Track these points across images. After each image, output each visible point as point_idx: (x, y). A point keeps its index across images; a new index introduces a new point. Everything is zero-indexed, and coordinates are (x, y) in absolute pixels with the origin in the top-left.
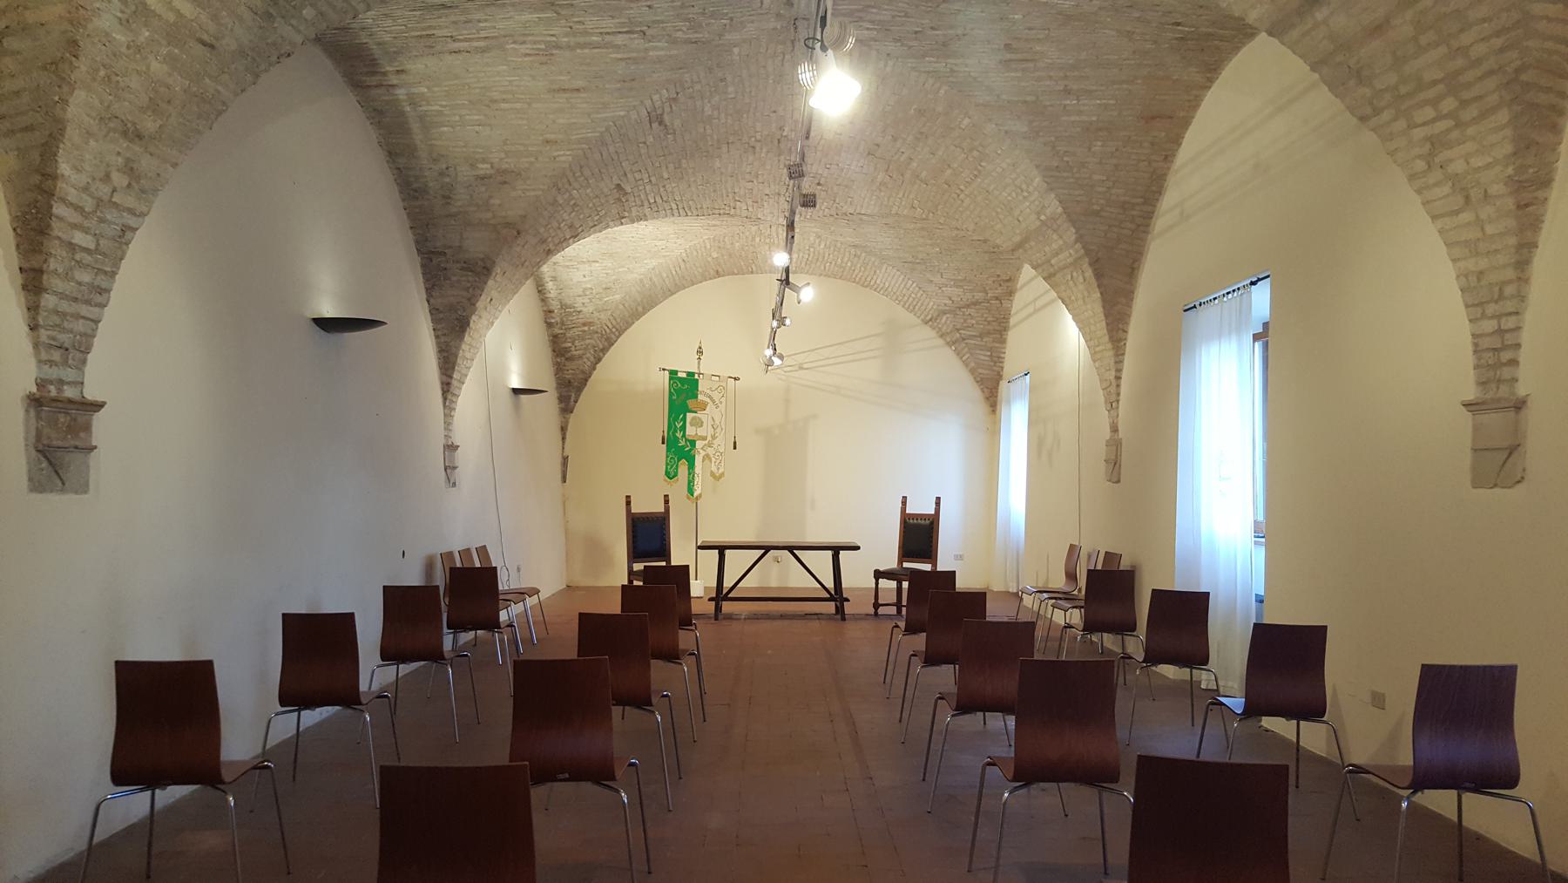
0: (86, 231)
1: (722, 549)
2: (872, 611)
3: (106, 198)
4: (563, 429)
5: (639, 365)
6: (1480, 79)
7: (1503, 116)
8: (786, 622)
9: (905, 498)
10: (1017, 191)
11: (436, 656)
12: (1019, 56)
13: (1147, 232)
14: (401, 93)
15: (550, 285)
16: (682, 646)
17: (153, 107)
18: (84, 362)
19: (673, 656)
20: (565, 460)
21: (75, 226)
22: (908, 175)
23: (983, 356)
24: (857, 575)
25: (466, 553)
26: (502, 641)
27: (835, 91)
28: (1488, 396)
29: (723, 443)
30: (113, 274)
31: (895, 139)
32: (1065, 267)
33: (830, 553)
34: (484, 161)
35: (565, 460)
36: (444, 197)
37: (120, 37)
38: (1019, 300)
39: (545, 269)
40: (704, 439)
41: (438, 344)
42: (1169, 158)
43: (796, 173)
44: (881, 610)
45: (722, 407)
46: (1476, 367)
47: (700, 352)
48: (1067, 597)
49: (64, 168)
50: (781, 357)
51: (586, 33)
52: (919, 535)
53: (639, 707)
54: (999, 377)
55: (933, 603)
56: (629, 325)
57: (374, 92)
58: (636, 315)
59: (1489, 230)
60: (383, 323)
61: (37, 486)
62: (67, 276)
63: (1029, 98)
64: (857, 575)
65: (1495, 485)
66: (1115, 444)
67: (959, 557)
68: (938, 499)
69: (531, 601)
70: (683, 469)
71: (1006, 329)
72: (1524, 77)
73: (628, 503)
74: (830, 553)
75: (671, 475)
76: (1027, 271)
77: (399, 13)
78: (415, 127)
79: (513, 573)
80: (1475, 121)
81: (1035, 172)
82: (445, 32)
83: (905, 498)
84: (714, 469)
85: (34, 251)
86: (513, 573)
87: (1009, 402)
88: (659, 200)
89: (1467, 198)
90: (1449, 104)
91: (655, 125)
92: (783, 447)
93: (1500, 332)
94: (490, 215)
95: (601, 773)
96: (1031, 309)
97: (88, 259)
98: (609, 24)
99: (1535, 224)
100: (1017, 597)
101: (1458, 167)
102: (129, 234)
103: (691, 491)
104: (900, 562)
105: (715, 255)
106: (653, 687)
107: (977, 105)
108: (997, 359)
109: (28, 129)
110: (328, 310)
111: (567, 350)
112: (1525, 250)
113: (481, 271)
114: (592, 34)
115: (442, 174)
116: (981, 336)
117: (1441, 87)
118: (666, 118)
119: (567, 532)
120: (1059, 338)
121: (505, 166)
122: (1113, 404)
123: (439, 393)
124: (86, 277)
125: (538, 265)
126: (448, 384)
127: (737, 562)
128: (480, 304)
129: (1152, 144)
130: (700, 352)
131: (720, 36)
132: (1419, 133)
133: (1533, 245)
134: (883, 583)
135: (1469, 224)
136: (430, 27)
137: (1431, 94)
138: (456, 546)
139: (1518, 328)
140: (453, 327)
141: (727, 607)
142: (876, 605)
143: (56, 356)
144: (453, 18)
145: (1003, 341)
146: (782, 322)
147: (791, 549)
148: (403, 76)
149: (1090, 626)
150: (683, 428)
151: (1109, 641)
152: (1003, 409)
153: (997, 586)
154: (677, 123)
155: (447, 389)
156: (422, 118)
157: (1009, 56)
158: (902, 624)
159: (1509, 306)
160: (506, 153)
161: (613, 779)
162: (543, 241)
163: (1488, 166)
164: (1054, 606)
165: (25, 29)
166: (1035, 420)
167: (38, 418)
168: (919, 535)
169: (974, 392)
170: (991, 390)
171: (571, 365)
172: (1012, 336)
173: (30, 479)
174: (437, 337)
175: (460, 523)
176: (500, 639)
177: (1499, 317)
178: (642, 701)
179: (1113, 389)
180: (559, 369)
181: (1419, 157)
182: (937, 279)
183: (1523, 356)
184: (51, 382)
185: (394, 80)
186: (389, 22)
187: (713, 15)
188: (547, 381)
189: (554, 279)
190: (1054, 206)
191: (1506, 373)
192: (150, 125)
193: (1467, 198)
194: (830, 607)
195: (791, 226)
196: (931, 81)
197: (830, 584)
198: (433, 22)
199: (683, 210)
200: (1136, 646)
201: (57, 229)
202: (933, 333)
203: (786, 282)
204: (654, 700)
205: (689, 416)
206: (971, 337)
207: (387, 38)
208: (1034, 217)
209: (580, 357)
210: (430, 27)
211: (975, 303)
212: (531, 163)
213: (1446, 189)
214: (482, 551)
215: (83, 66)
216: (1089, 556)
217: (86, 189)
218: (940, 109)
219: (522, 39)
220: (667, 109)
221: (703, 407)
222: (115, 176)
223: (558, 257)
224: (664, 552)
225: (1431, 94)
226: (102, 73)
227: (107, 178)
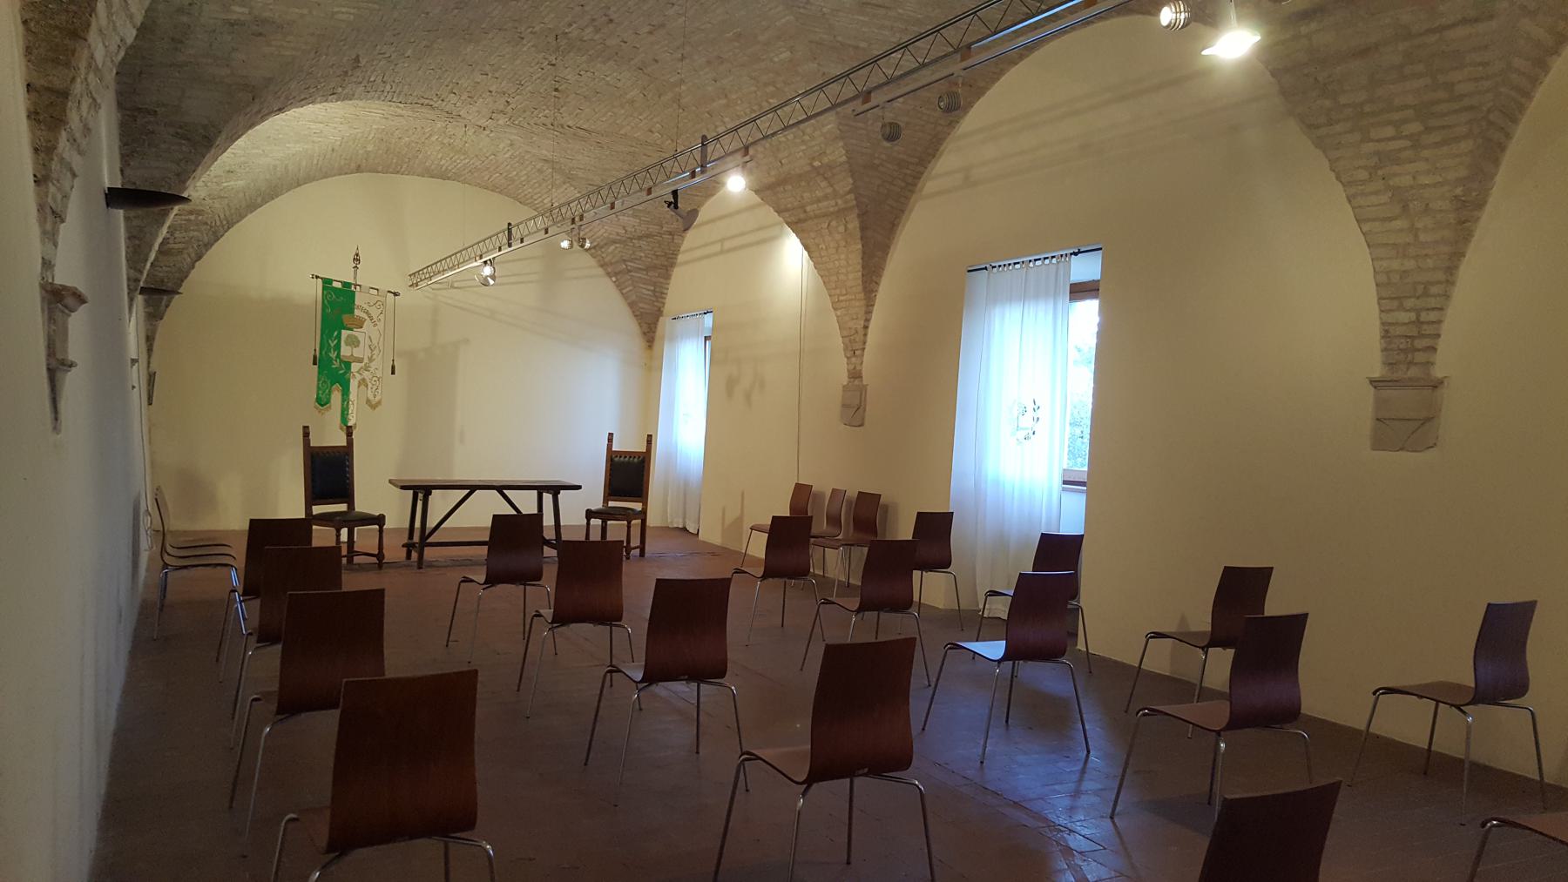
6: (1456, 111)
7: (1466, 146)
13: (912, 192)
23: (646, 291)
28: (1395, 377)
29: (380, 366)
32: (825, 215)
40: (360, 360)
45: (381, 325)
46: (1384, 350)
47: (357, 259)
54: (659, 313)
56: (242, 217)
58: (252, 206)
59: (1422, 237)
65: (1402, 449)
70: (336, 397)
71: (673, 265)
72: (1491, 117)
80: (1437, 145)
84: (371, 397)
85: (56, 61)
87: (673, 339)
89: (1405, 208)
90: (1415, 127)
92: (428, 374)
93: (1418, 323)
99: (1467, 237)
101: (1406, 181)
104: (606, 500)
105: (370, 148)
108: (659, 295)
112: (1457, 255)
115: (181, 10)
116: (647, 269)
117: (1410, 113)
121: (267, 14)
122: (854, 347)
127: (440, 503)
130: (357, 259)
132: (1370, 147)
134: (593, 521)
135: (1401, 230)
137: (1396, 116)
139: (1440, 322)
141: (429, 553)
145: (668, 277)
159: (1432, 302)
163: (1435, 185)
169: (631, 326)
170: (650, 324)
172: (677, 273)
177: (1418, 311)
179: (859, 338)
181: (1365, 168)
183: (1441, 345)
191: (1420, 357)
193: (1405, 208)
202: (593, 262)
205: (345, 333)
209: (180, 252)
211: (648, 236)
212: (302, 16)
213: (1384, 198)
221: (360, 324)
225: (1396, 116)
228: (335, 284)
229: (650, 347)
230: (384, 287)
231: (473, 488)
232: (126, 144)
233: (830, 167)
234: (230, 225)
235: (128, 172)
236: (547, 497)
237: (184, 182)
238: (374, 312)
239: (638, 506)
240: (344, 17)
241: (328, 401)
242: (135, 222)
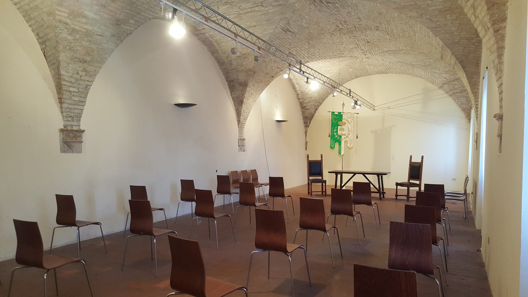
0: (74, 87)
3: (79, 78)
4: (306, 133)
15: (297, 86)
17: (88, 54)
18: (80, 120)
20: (306, 143)
21: (69, 86)
24: (389, 184)
29: (352, 136)
30: (86, 98)
35: (306, 143)
37: (70, 38)
40: (345, 135)
41: (236, 109)
44: (398, 197)
47: (343, 105)
49: (63, 72)
61: (63, 151)
62: (70, 99)
68: (423, 156)
70: (337, 145)
75: (332, 148)
78: (215, 44)
84: (349, 145)
91: (288, 32)
92: (382, 137)
94: (244, 68)
97: (76, 94)
99: (502, 38)
102: (89, 87)
103: (340, 153)
104: (409, 180)
107: (393, 9)
109: (54, 64)
110: (182, 101)
111: (305, 107)
113: (244, 85)
115: (227, 57)
123: (237, 123)
124: (76, 99)
127: (346, 177)
130: (343, 105)
133: (503, 47)
143: (70, 119)
150: (337, 131)
165: (49, 39)
167: (63, 135)
169: (461, 114)
171: (307, 112)
173: (61, 150)
182: (437, 71)
184: (69, 126)
185: (203, 31)
189: (297, 84)
192: (88, 58)
201: (64, 88)
202: (443, 92)
205: (339, 127)
206: (457, 93)
209: (310, 109)
215: (61, 47)
217: (71, 77)
222: (80, 73)
226: (68, 47)
227: (78, 73)
231: (355, 174)
236: (339, 176)
238: (349, 120)
239: (418, 182)
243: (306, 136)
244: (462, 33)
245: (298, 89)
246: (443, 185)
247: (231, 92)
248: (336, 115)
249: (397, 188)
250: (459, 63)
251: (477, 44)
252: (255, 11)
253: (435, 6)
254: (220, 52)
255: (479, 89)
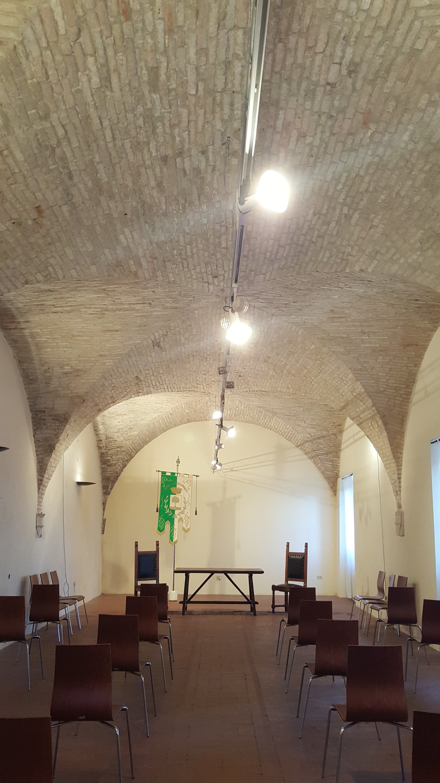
1: (187, 573)
2: (271, 610)
4: (104, 504)
5: (146, 469)
8: (223, 616)
9: (288, 543)
10: (339, 382)
11: (19, 637)
12: (338, 315)
14: (27, 332)
15: (101, 427)
16: (160, 633)
19: (154, 639)
20: (104, 521)
22: (285, 372)
23: (329, 465)
24: (263, 588)
25: (44, 576)
26: (60, 627)
27: (238, 332)
29: (189, 512)
31: (278, 354)
32: (368, 419)
33: (247, 575)
34: (68, 365)
35: (104, 521)
36: (46, 383)
38: (346, 436)
39: (99, 418)
40: (179, 509)
41: (38, 459)
42: (417, 365)
43: (223, 371)
44: (276, 609)
45: (190, 491)
47: (178, 462)
48: (378, 602)
50: (221, 465)
51: (121, 304)
52: (296, 565)
53: (132, 672)
54: (336, 477)
55: (302, 605)
56: (141, 447)
57: (13, 331)
58: (145, 442)
60: (8, 449)
63: (344, 336)
64: (263, 588)
66: (400, 515)
67: (320, 578)
68: (306, 544)
69: (79, 604)
70: (167, 526)
71: (340, 450)
73: (136, 546)
74: (247, 575)
75: (161, 530)
76: (349, 421)
77: (27, 293)
78: (33, 348)
79: (71, 586)
81: (349, 371)
82: (50, 303)
83: (288, 543)
84: (184, 526)
86: (71, 586)
88: (158, 384)
91: (156, 347)
92: (222, 512)
95: (103, 716)
96: (352, 440)
98: (133, 300)
100: (352, 601)
103: (171, 538)
104: (287, 581)
105: (187, 411)
106: (140, 660)
108: (335, 467)
111: (108, 461)
113: (62, 420)
114: (125, 304)
115: (46, 371)
118: (162, 344)
119: (103, 562)
120: (367, 456)
121: (78, 368)
122: (397, 492)
123: (36, 485)
125: (94, 417)
126: (42, 480)
127: (196, 580)
128: (61, 438)
129: (408, 358)
130: (178, 462)
131: (188, 305)
134: (277, 593)
136: (43, 301)
138: (39, 572)
140: (46, 449)
141: (190, 607)
142: (274, 606)
144: (54, 296)
146: (220, 446)
147: (226, 573)
148: (28, 324)
149: (392, 620)
150: (168, 503)
151: (403, 628)
152: (340, 494)
153: (341, 595)
154: (167, 346)
155: (41, 483)
156: (37, 344)
157: (332, 316)
158: (286, 619)
160: (79, 361)
161: (111, 720)
162: (97, 405)
164: (372, 608)
166: (358, 499)
168: (296, 565)
170: (333, 482)
171: (110, 469)
172: (344, 455)
174: (37, 455)
175: (41, 559)
176: (60, 627)
178: (133, 668)
179: (397, 484)
180: (103, 471)
182: (302, 424)
186: (22, 298)
187: (185, 296)
188: (96, 478)
189: (103, 424)
190: (360, 388)
194: (247, 608)
195: (223, 398)
196: (294, 327)
197: (247, 593)
198: (45, 298)
199: (170, 388)
200: (417, 632)
202: (301, 452)
203: (221, 426)
204: (141, 668)
205: (172, 496)
207: (21, 305)
208: (349, 393)
209: (115, 464)
210: (43, 301)
212: (92, 366)
214: (54, 574)
216: (390, 578)
218: (299, 340)
219: (89, 306)
220: (162, 340)
223: (106, 412)
224: (155, 574)
228: (167, 474)
229: (335, 495)
230: (191, 473)
231: (212, 573)
232: (34, 425)
233: (359, 394)
234: (137, 451)
235: (36, 436)
237: (58, 438)
238: (186, 485)
240: (109, 364)
241: (163, 530)
242: (40, 456)
243: (104, 509)
244: (390, 381)
245: (102, 432)
246: (315, 588)
247: (35, 431)
248: (168, 476)
249: (274, 593)
250: (381, 418)
251: (405, 396)
252: (134, 309)
253: (370, 343)
254: (36, 362)
255: (401, 453)
